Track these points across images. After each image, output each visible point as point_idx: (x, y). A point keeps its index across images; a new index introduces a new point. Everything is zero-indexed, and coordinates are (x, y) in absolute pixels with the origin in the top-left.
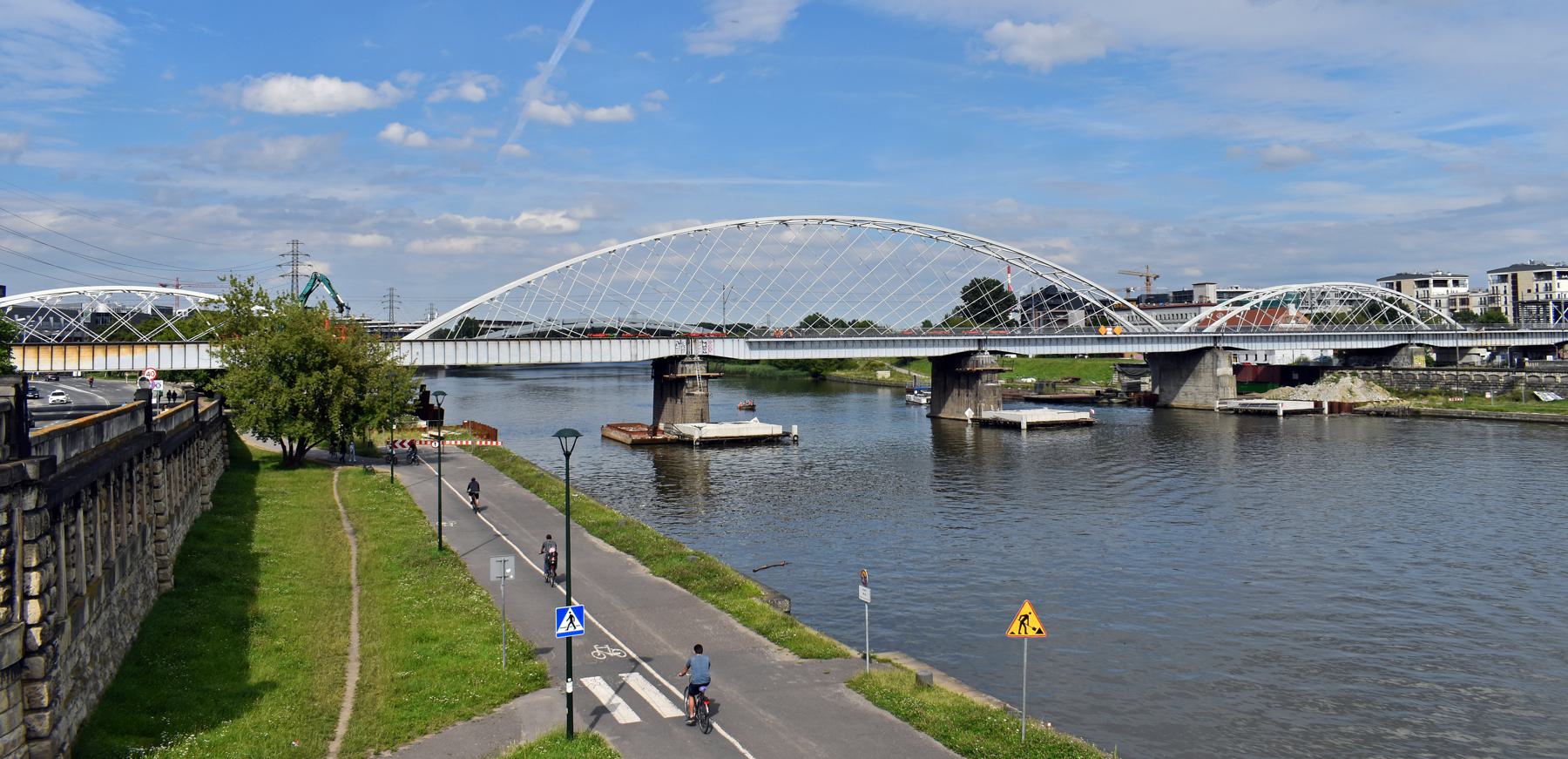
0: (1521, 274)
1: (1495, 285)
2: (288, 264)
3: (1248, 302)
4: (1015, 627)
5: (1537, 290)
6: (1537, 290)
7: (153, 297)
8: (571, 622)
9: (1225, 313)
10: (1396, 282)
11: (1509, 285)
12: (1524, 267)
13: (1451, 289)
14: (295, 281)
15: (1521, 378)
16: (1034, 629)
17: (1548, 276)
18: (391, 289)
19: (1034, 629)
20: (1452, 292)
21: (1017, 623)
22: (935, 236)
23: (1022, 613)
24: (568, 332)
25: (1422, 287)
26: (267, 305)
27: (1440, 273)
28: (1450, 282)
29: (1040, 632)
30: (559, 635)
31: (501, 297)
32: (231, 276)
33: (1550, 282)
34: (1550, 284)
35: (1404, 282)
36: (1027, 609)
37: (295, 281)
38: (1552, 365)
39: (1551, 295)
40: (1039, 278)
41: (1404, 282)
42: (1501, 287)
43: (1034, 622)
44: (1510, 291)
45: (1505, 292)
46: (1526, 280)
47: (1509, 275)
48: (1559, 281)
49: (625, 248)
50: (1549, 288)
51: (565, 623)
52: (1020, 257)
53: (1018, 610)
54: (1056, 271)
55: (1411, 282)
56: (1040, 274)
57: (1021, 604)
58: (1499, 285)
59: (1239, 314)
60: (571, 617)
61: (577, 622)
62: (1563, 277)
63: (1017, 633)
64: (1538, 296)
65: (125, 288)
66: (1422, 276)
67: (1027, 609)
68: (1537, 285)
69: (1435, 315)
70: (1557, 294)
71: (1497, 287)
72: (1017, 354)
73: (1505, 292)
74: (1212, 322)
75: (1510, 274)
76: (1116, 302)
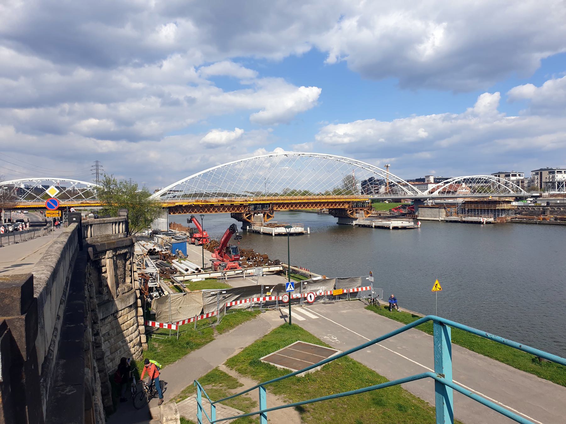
0: (543, 172)
1: (534, 176)
2: (94, 169)
3: (449, 182)
4: (434, 288)
5: (549, 178)
6: (549, 178)
7: (39, 182)
8: (290, 287)
9: (441, 186)
10: (498, 174)
11: (539, 176)
12: (545, 170)
13: (518, 177)
14: (97, 175)
15: (548, 209)
16: (439, 288)
17: (554, 173)
18: (130, 179)
19: (439, 288)
20: (518, 179)
21: (434, 287)
22: (339, 160)
23: (436, 284)
24: (210, 194)
25: (507, 177)
26: (116, 185)
27: (514, 172)
28: (517, 175)
29: (440, 289)
30: (287, 291)
31: (186, 182)
32: (105, 174)
33: (554, 175)
34: (554, 176)
35: (501, 175)
36: (437, 282)
37: (97, 175)
38: (560, 204)
39: (554, 180)
40: (376, 174)
41: (501, 175)
42: (536, 177)
43: (439, 286)
44: (539, 178)
45: (537, 178)
46: (545, 174)
47: (539, 173)
48: (557, 174)
49: (231, 164)
50: (553, 177)
51: (289, 287)
52: (369, 167)
53: (434, 283)
54: (382, 172)
55: (504, 175)
56: (376, 173)
57: (435, 281)
58: (535, 176)
59: (447, 187)
60: (290, 285)
61: (292, 287)
62: (558, 173)
63: (434, 290)
64: (549, 180)
65: (47, 179)
66: (507, 173)
67: (437, 282)
68: (549, 176)
69: (515, 187)
70: (556, 179)
71: (535, 177)
72: (555, 203)
73: (537, 178)
74: (437, 190)
75: (539, 172)
76: (403, 183)
